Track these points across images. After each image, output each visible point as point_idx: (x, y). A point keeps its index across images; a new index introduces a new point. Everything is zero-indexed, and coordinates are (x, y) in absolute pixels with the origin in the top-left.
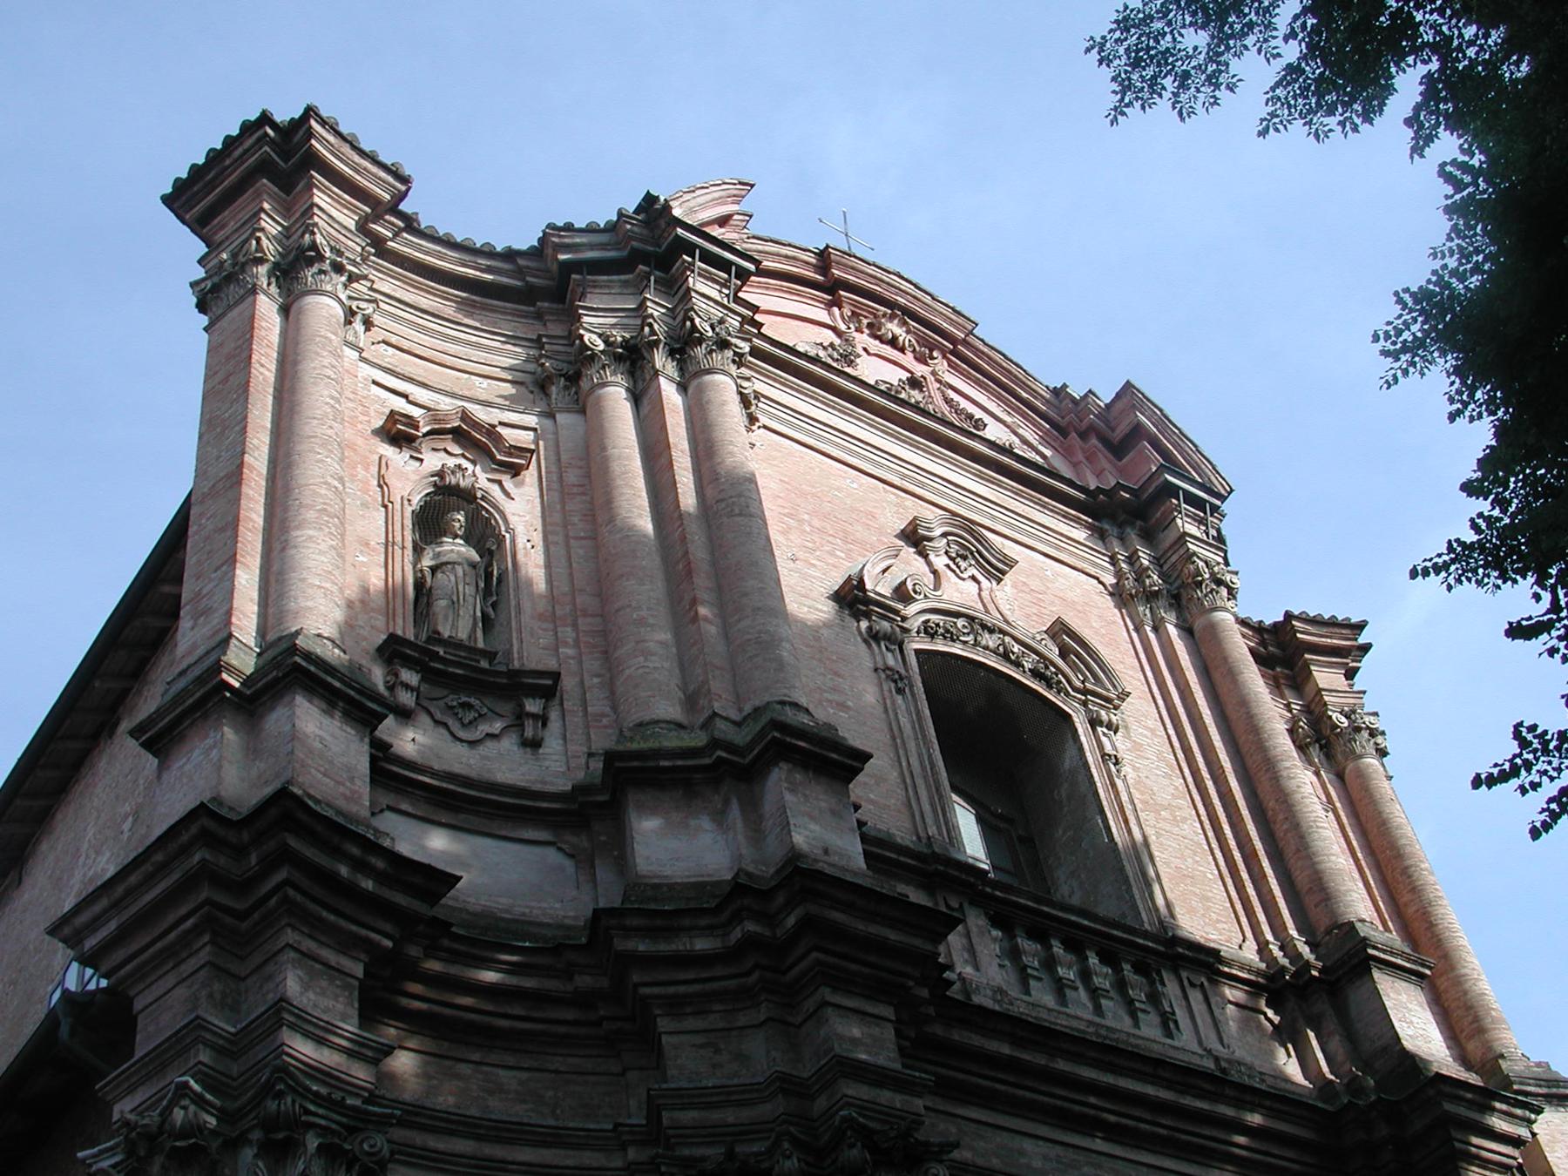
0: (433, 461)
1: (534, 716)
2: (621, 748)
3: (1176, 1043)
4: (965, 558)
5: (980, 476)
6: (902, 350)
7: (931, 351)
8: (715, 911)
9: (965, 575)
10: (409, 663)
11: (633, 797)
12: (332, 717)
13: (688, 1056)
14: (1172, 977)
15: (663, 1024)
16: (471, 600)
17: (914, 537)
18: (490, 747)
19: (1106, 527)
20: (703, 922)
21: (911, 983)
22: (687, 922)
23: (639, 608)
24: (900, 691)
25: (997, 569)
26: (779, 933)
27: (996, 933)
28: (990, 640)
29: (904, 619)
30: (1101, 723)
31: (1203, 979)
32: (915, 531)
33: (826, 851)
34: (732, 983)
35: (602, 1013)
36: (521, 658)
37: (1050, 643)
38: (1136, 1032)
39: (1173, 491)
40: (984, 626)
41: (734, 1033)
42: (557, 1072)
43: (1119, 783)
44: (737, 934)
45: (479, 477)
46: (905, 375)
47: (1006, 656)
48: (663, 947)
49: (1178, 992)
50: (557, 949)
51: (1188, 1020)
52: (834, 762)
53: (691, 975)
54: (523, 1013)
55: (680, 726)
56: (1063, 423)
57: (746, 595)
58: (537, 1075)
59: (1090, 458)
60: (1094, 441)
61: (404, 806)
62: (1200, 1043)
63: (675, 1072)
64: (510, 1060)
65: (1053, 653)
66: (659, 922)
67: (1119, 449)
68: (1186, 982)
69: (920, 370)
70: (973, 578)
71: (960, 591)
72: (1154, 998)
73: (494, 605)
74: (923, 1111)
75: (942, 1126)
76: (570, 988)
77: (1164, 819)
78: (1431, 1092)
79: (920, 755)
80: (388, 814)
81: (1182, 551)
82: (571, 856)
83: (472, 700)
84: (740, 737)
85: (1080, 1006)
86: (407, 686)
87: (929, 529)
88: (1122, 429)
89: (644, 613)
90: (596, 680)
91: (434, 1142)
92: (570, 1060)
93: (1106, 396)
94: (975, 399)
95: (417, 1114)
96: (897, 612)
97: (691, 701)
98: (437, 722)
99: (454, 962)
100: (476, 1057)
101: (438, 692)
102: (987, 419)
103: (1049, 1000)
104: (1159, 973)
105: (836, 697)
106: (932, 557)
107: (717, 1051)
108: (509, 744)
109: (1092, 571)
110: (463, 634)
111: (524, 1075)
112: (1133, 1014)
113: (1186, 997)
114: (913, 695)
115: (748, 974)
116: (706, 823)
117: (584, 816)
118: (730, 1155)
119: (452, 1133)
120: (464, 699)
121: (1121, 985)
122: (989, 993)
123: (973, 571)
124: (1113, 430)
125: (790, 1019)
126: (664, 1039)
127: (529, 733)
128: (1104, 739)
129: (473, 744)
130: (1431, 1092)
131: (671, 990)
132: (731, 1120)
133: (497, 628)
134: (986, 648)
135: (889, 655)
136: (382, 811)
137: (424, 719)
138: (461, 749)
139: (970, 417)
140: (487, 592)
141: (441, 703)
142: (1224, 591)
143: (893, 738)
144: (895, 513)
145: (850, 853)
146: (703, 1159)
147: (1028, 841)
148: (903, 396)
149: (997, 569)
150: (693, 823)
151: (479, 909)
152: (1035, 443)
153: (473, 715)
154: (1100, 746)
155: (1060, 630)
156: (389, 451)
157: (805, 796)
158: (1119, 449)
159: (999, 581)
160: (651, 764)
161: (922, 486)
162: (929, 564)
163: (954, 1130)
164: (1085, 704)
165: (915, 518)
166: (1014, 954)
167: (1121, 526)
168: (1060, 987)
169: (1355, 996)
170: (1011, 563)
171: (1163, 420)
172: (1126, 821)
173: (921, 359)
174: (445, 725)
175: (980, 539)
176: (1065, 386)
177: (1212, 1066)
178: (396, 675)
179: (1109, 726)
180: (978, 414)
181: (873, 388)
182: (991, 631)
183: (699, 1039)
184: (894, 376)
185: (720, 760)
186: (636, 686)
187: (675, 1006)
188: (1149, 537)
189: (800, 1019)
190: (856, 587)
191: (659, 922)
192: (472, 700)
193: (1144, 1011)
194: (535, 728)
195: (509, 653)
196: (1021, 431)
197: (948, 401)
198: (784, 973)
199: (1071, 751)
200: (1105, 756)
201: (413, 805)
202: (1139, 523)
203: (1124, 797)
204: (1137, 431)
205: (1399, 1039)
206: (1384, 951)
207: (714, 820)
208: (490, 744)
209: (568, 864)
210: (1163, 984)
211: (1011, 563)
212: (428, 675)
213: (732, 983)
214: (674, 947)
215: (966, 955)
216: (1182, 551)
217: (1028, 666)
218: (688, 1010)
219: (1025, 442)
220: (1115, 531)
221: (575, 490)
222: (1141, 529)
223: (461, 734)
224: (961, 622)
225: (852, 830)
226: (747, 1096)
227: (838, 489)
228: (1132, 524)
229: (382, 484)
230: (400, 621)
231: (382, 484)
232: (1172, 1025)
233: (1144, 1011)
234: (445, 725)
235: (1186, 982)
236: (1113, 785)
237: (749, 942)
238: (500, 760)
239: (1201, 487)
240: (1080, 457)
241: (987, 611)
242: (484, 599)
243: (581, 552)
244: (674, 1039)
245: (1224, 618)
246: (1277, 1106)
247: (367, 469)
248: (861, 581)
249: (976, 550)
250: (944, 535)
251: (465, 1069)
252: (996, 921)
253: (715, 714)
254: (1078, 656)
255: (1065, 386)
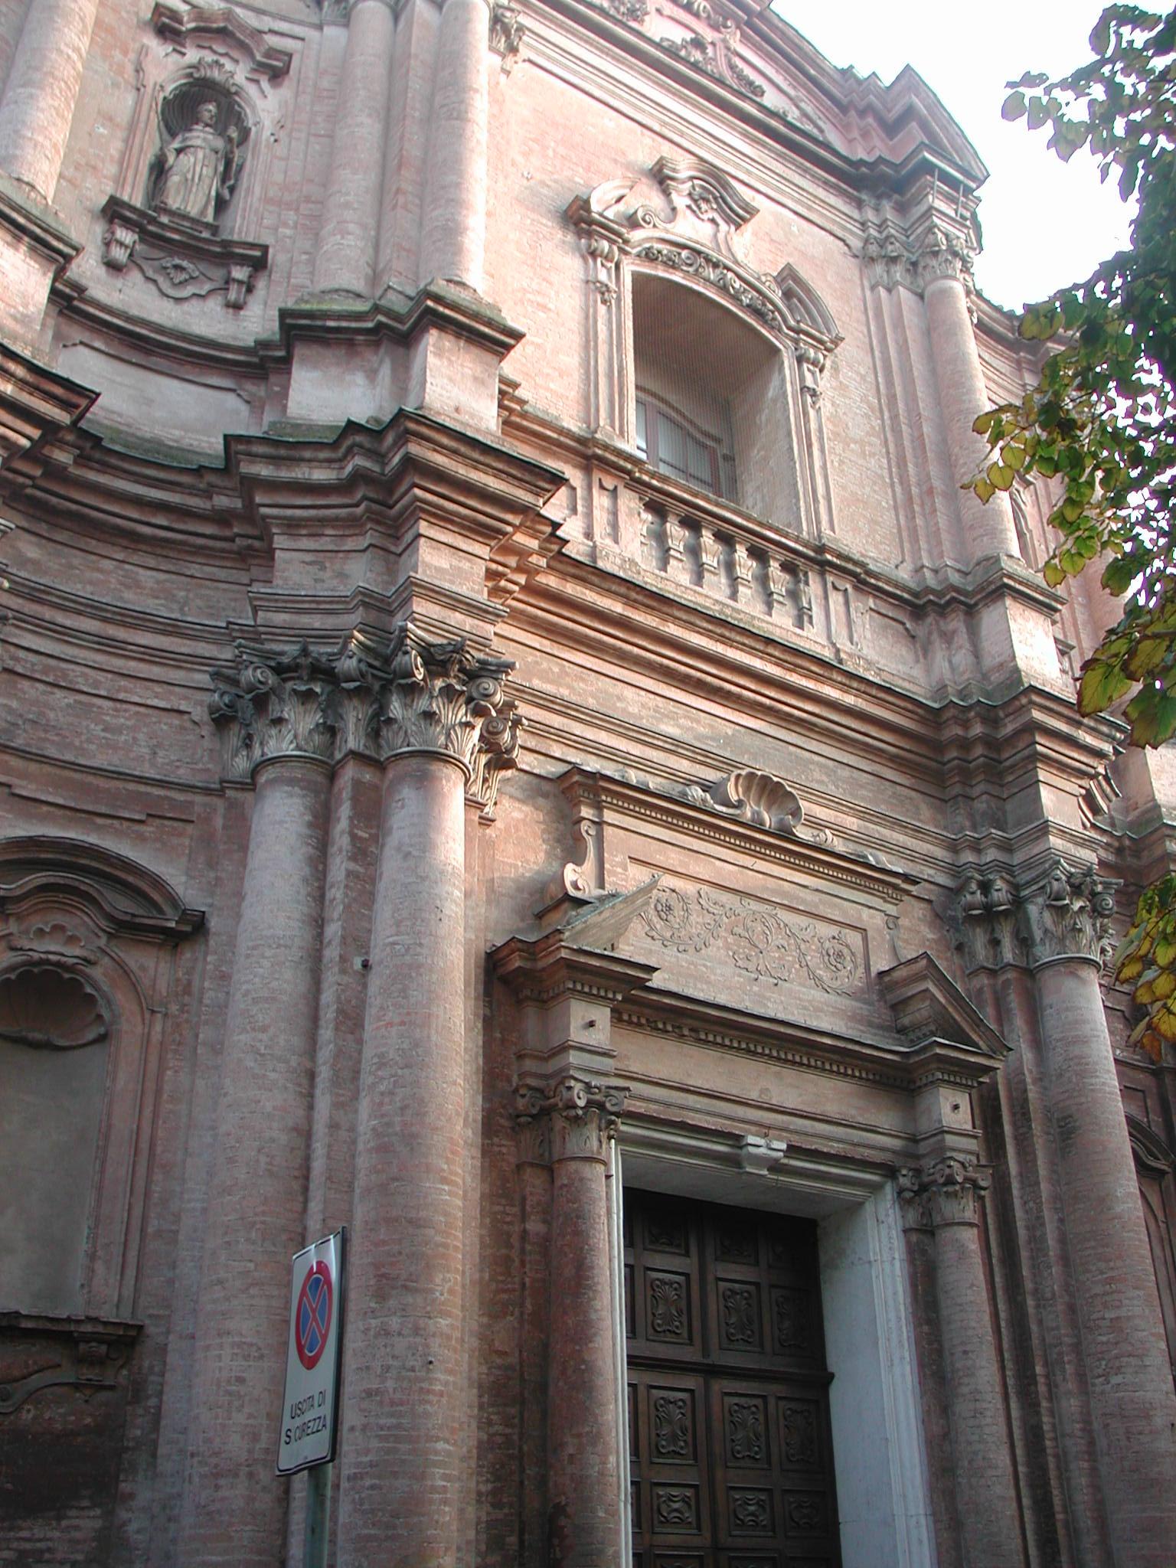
0: (192, 55)
1: (240, 282)
2: (296, 307)
3: (804, 633)
4: (707, 201)
5: (745, 135)
6: (697, 15)
7: (726, 19)
8: (334, 445)
9: (705, 217)
10: (128, 224)
11: (299, 351)
12: (17, 249)
13: (295, 569)
14: (818, 579)
15: (279, 541)
16: (207, 181)
17: (661, 177)
18: (194, 306)
19: (864, 197)
20: (322, 455)
21: (509, 529)
22: (307, 454)
23: (348, 194)
24: (604, 302)
25: (739, 216)
26: (387, 469)
27: (648, 517)
28: (712, 274)
29: (626, 242)
30: (808, 360)
31: (848, 586)
32: (660, 170)
33: (457, 410)
34: (343, 512)
35: (236, 530)
36: (240, 233)
37: (774, 286)
38: (767, 618)
39: (928, 168)
40: (708, 260)
41: (341, 555)
42: (192, 577)
43: (812, 413)
44: (349, 468)
45: (237, 72)
46: (689, 36)
47: (724, 289)
48: (285, 474)
49: (820, 592)
50: (200, 471)
51: (823, 618)
52: (491, 338)
53: (308, 502)
54: (165, 523)
55: (359, 296)
56: (845, 101)
57: (443, 188)
58: (174, 577)
59: (865, 134)
60: (870, 120)
61: (97, 344)
62: (829, 637)
63: (280, 582)
64: (151, 562)
65: (777, 296)
66: (283, 452)
67: (891, 129)
68: (829, 586)
69: (709, 35)
70: (713, 221)
71: (693, 228)
72: (794, 595)
73: (232, 189)
74: (492, 637)
75: (545, 665)
76: (208, 505)
77: (852, 451)
78: (1024, 701)
79: (611, 359)
80: (81, 348)
81: (927, 224)
82: (248, 402)
83: (185, 264)
84: (401, 306)
85: (713, 594)
86: (121, 244)
87: (674, 170)
88: (898, 110)
89: (350, 198)
90: (304, 257)
91: (61, 618)
92: (207, 569)
93: (887, 79)
94: (756, 65)
95: (49, 593)
96: (620, 235)
97: (375, 278)
98: (148, 279)
99: (105, 473)
100: (120, 556)
101: (157, 254)
102: (766, 86)
103: (685, 579)
104: (806, 574)
105: (539, 299)
106: (674, 196)
107: (323, 568)
108: (214, 305)
109: (840, 233)
110: (193, 210)
111: (162, 576)
112: (769, 605)
113: (826, 598)
114: (619, 307)
115: (357, 505)
116: (360, 378)
117: (261, 367)
118: (305, 652)
119: (80, 613)
120: (177, 261)
121: (763, 580)
122: (618, 561)
123: (711, 215)
124: (889, 111)
125: (393, 549)
126: (278, 553)
127: (232, 296)
128: (808, 375)
129: (178, 300)
130: (1024, 701)
131: (289, 512)
132: (317, 625)
133: (231, 209)
134: (707, 280)
135: (604, 271)
136: (75, 345)
137: (136, 276)
138: (168, 305)
139: (751, 84)
140: (224, 178)
141: (156, 263)
142: (959, 265)
143: (587, 341)
144: (646, 152)
145: (483, 417)
146: (282, 654)
147: (729, 459)
148: (683, 53)
149: (739, 216)
150: (348, 378)
151: (148, 436)
152: (815, 117)
153: (184, 276)
154: (802, 378)
155: (788, 278)
156: (152, 42)
157: (449, 360)
158: (891, 129)
159: (738, 227)
160: (319, 323)
161: (682, 135)
162: (670, 202)
163: (556, 670)
164: (796, 342)
165: (662, 158)
166: (660, 537)
167: (879, 197)
168: (699, 573)
169: (988, 617)
170: (752, 211)
171: (935, 105)
172: (810, 446)
173: (715, 28)
174: (155, 282)
175: (725, 186)
176: (851, 67)
177: (832, 656)
178: (113, 233)
179: (815, 363)
180: (759, 81)
181: (658, 46)
182: (716, 265)
183: (309, 557)
184: (678, 35)
185: (380, 325)
186: (328, 260)
187: (292, 526)
188: (902, 209)
189: (400, 549)
190: (582, 208)
191: (283, 452)
192: (185, 264)
193: (779, 602)
194: (239, 293)
195: (233, 229)
196: (802, 105)
197: (732, 67)
198: (391, 507)
199: (775, 382)
200: (804, 388)
201: (107, 344)
202: (896, 197)
203: (813, 426)
204: (909, 113)
205: (1014, 657)
206: (1020, 583)
207: (367, 377)
208: (194, 301)
209: (244, 408)
210: (807, 583)
211: (752, 211)
212: (145, 236)
213: (343, 512)
214: (293, 475)
215: (609, 530)
216: (927, 224)
217: (746, 301)
218: (304, 532)
219: (805, 115)
220: (873, 201)
221: (325, 94)
222: (896, 203)
223: (170, 292)
224: (685, 253)
225: (492, 397)
226: (335, 606)
227: (593, 125)
228: (889, 197)
229: (139, 70)
230: (128, 189)
231: (139, 70)
232: (806, 618)
233: (779, 602)
234: (155, 282)
235: (829, 586)
236: (806, 414)
237: (359, 477)
238: (205, 319)
239: (959, 169)
240: (856, 134)
241: (719, 251)
242: (223, 181)
243: (317, 147)
244: (288, 555)
245: (958, 288)
246: (882, 695)
247: (125, 53)
248: (587, 202)
249: (717, 192)
250: (692, 178)
251: (107, 564)
252: (651, 506)
253: (389, 287)
254: (800, 301)
255: (851, 67)
